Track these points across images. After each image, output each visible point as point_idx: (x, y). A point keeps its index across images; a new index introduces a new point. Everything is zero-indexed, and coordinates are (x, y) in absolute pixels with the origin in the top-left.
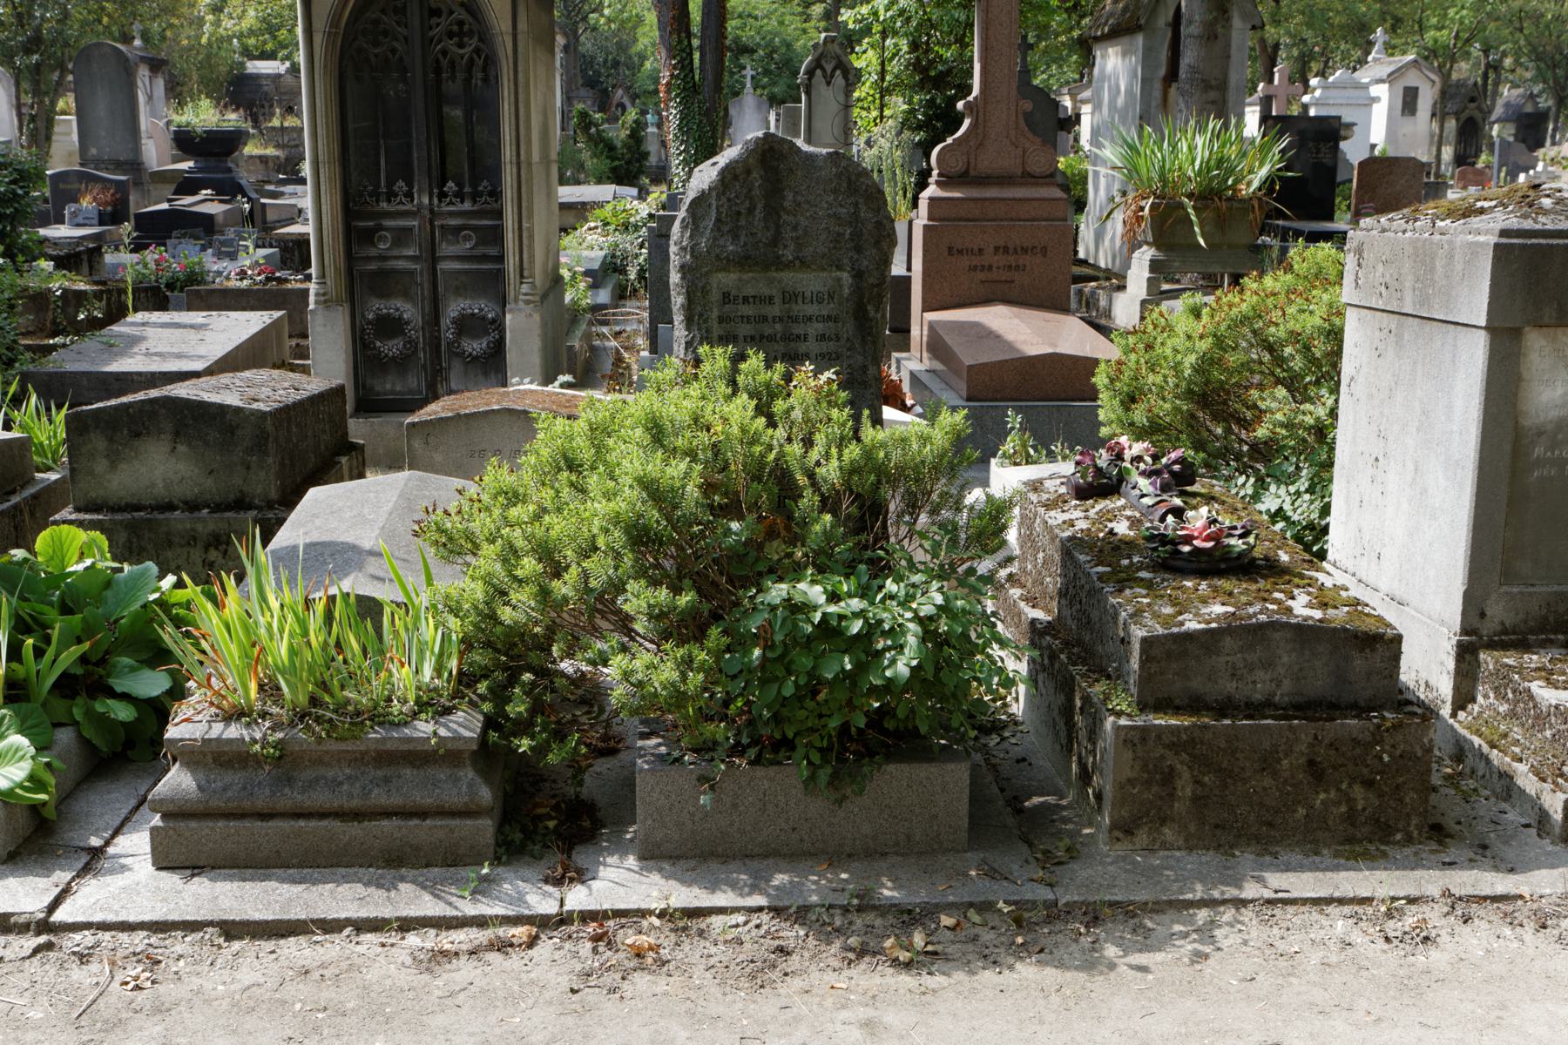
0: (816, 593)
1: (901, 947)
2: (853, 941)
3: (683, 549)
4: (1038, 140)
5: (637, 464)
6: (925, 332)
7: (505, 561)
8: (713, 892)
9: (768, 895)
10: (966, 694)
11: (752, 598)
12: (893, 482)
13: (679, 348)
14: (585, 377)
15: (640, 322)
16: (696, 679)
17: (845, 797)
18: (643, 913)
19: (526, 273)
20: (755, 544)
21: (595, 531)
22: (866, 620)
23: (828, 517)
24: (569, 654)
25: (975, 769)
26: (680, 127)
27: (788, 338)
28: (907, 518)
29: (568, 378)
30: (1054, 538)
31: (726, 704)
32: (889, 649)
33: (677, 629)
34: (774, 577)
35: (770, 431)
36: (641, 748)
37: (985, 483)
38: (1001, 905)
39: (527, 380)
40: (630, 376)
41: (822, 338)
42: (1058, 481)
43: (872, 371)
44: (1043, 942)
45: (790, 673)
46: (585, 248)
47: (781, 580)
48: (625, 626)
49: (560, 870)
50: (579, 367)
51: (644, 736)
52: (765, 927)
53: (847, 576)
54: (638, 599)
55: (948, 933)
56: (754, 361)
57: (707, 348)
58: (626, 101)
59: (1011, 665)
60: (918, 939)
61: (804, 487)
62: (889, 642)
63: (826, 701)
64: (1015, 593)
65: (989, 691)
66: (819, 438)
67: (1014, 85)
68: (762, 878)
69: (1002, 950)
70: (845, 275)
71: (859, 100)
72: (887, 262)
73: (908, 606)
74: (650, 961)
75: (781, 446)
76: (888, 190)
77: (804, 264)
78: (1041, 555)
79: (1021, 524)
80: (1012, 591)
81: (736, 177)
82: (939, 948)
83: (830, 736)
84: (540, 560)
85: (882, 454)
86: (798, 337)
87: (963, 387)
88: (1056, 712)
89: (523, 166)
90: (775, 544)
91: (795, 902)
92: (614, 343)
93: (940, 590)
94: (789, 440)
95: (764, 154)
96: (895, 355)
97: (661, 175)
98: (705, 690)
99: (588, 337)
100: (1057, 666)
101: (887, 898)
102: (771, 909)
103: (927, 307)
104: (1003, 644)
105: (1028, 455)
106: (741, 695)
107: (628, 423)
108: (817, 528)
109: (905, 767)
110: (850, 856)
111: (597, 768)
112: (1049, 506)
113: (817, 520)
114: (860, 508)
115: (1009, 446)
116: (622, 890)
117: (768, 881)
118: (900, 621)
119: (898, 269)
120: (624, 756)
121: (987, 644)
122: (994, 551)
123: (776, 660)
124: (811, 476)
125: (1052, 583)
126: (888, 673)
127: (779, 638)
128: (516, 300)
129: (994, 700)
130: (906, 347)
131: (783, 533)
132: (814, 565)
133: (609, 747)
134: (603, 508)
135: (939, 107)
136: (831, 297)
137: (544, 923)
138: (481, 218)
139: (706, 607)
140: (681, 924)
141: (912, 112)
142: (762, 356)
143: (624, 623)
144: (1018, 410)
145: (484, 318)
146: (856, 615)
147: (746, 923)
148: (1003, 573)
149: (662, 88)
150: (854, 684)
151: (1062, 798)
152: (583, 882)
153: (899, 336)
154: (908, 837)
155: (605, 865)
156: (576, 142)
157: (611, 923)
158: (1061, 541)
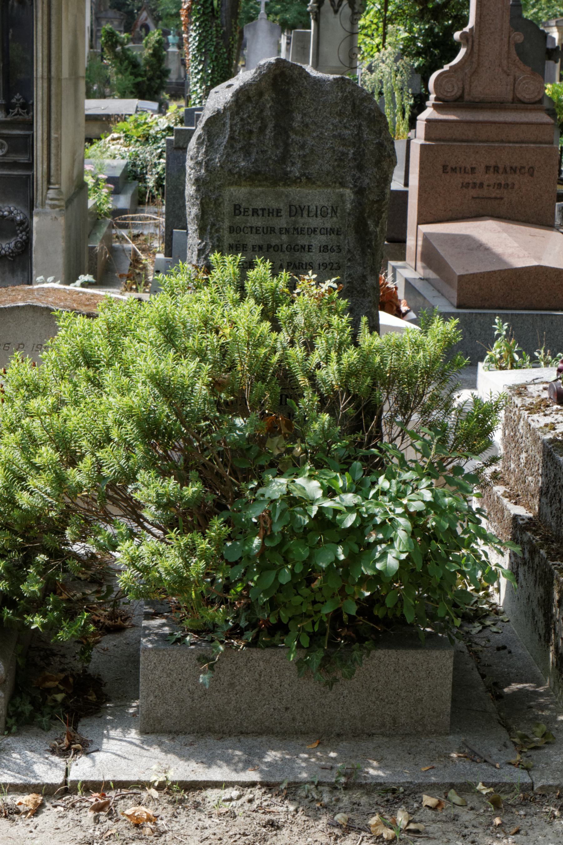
0: (312, 488)
1: (386, 825)
2: (340, 817)
3: (190, 442)
4: (529, 69)
5: (150, 362)
6: (420, 243)
7: (24, 449)
8: (209, 767)
9: (261, 771)
10: (452, 584)
11: (254, 491)
12: (388, 384)
13: (192, 255)
14: (104, 277)
15: (157, 226)
16: (198, 566)
17: (336, 680)
18: (143, 785)
19: (53, 180)
20: (257, 441)
21: (109, 423)
22: (360, 514)
23: (326, 417)
24: (82, 537)
25: (458, 655)
26: (199, 48)
27: (293, 248)
28: (399, 418)
29: (88, 278)
30: (536, 440)
31: (227, 588)
32: (380, 542)
33: (182, 518)
34: (275, 471)
35: (274, 335)
36: (146, 628)
37: (473, 385)
38: (480, 786)
39: (50, 279)
40: (146, 276)
41: (325, 249)
42: (541, 387)
43: (370, 281)
44: (519, 823)
45: (287, 562)
46: (109, 156)
47: (280, 474)
48: (135, 513)
49: (66, 741)
50: (99, 267)
51: (149, 616)
52: (257, 802)
53: (342, 472)
54: (148, 489)
55: (430, 812)
56: (262, 269)
57: (218, 255)
58: (150, 22)
59: (494, 558)
60: (401, 818)
61: (305, 387)
62: (381, 536)
63: (320, 589)
64: (499, 489)
65: (473, 580)
66: (320, 343)
67: (507, 18)
68: (256, 754)
69: (480, 830)
70: (348, 191)
71: (364, 27)
72: (387, 179)
73: (399, 501)
74: (148, 831)
75: (284, 349)
76: (387, 111)
77: (310, 180)
78: (524, 455)
79: (506, 426)
80: (496, 488)
81: (249, 99)
82: (421, 827)
83: (322, 622)
84: (57, 449)
85: (378, 359)
86: (303, 247)
87: (454, 294)
88: (535, 603)
89: (54, 82)
90: (276, 440)
91: (286, 779)
92: (131, 245)
93: (429, 487)
94: (292, 343)
95: (275, 78)
96: (392, 263)
97: (180, 91)
98: (207, 575)
99: (108, 238)
100: (537, 560)
101: (373, 777)
102: (263, 784)
103: (422, 220)
104: (487, 539)
105: (513, 360)
106: (240, 580)
107: (143, 323)
108: (316, 426)
109: (392, 652)
110: (338, 735)
111: (104, 645)
112: (532, 410)
113: (315, 419)
114: (356, 408)
115: (496, 351)
116: (123, 762)
117: (261, 757)
118: (392, 515)
119: (396, 185)
120: (129, 633)
121: (472, 539)
122: (481, 451)
123: (273, 549)
124: (312, 377)
125: (534, 481)
126: (379, 566)
127: (277, 529)
128: (43, 204)
129: (477, 591)
130: (402, 257)
131: (284, 430)
132: (313, 461)
133: (116, 625)
134: (118, 401)
135: (437, 35)
136: (334, 211)
137: (49, 792)
138: (14, 128)
139: (210, 499)
140: (178, 797)
141: (413, 39)
142: (268, 264)
143: (134, 510)
144: (504, 318)
145: (13, 220)
146: (350, 509)
147: (239, 797)
148: (489, 471)
149: (183, 12)
150: (347, 573)
151: (539, 685)
152: (87, 754)
153: (396, 246)
154: (394, 720)
155: (108, 738)
156: (102, 59)
157: (112, 794)
158: (543, 443)
